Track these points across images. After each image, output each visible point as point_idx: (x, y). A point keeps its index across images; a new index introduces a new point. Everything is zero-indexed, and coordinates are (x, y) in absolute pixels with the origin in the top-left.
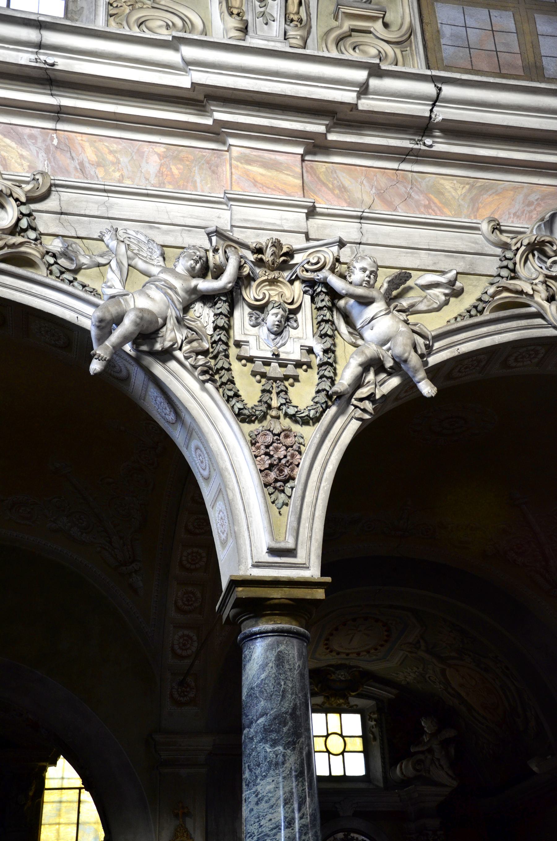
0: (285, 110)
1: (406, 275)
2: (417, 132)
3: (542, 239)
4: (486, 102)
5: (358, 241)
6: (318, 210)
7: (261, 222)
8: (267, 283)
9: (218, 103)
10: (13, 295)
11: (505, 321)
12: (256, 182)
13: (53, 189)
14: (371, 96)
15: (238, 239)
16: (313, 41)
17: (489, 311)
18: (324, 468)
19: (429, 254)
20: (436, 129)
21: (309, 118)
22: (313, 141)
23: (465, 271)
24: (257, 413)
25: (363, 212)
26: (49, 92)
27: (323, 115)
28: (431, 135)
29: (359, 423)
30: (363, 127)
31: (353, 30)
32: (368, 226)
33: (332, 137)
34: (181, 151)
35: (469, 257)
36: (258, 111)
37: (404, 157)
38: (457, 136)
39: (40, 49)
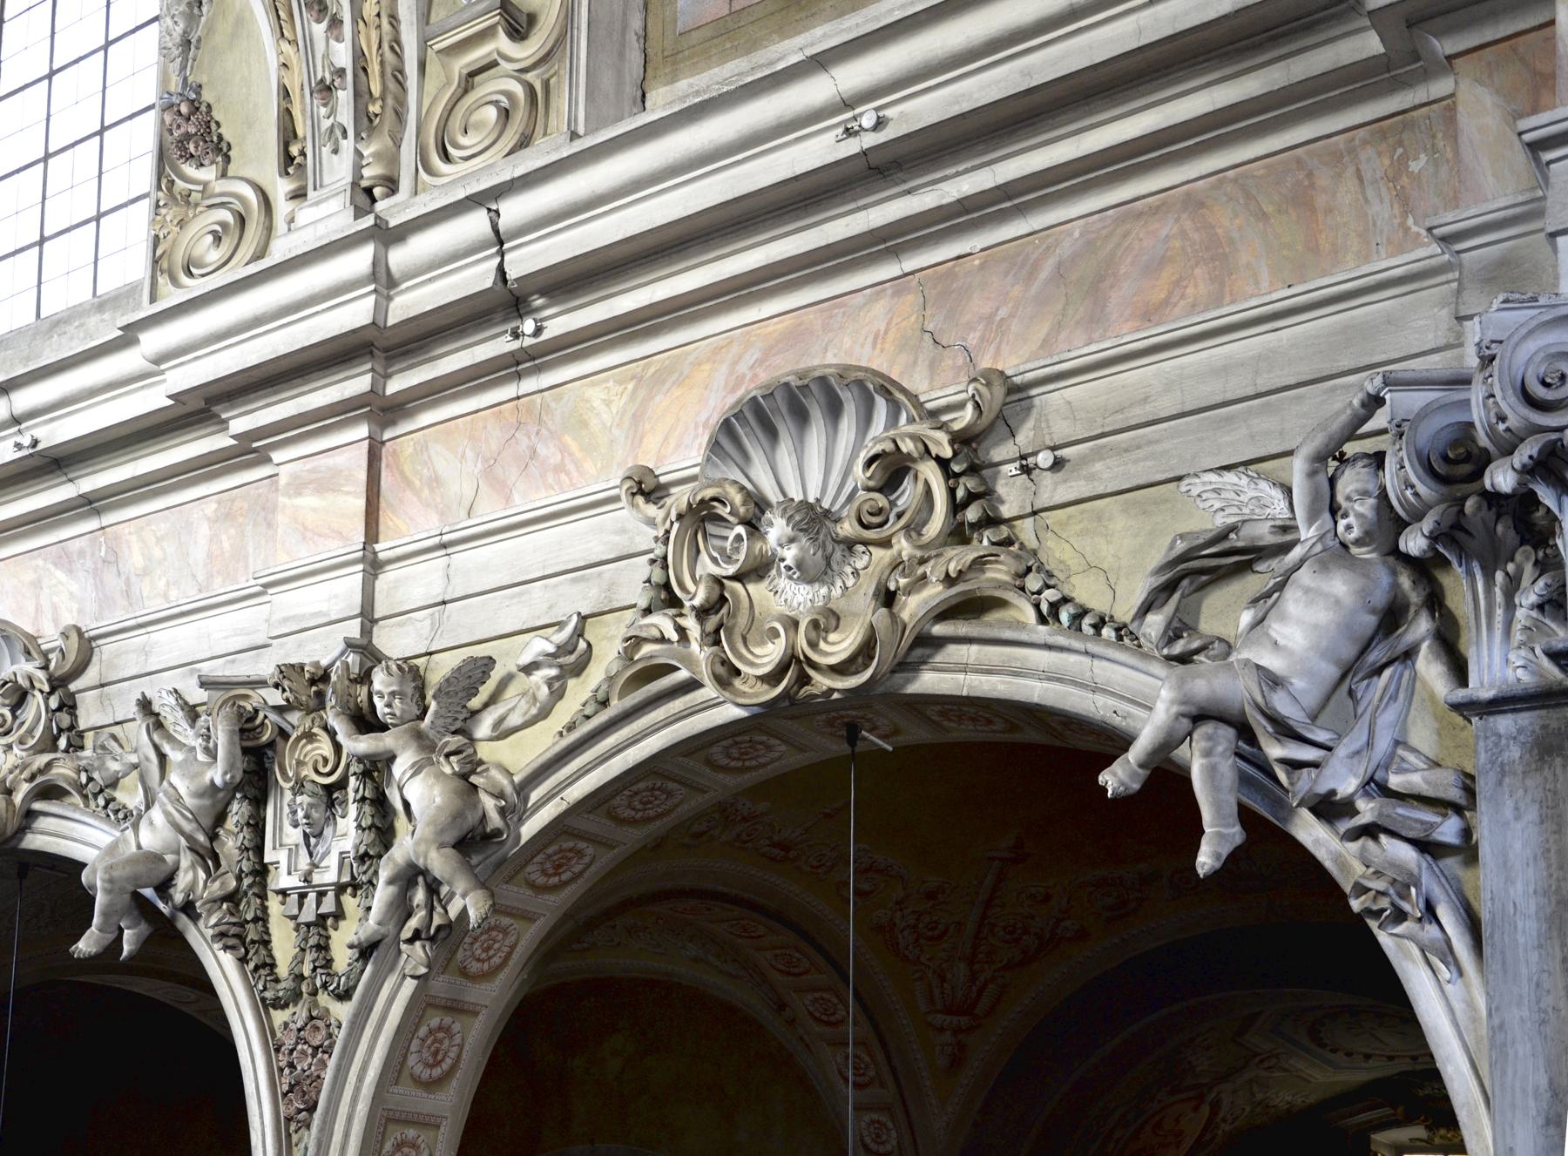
0: (307, 374)
1: (479, 663)
2: (508, 313)
3: (698, 498)
4: (576, 204)
5: (440, 599)
6: (382, 556)
7: (302, 617)
8: (304, 741)
9: (224, 405)
10: (58, 844)
11: (646, 710)
12: (306, 529)
13: (94, 645)
14: (404, 286)
15: (249, 677)
16: (410, 145)
17: (616, 698)
18: (360, 1079)
19: (546, 586)
20: (532, 294)
21: (342, 371)
22: (368, 409)
23: (596, 610)
24: (281, 994)
25: (441, 534)
26: (64, 478)
27: (356, 357)
28: (530, 309)
29: (415, 982)
30: (427, 345)
31: (472, 74)
32: (464, 558)
33: (394, 386)
34: (233, 500)
35: (610, 570)
36: (276, 393)
37: (513, 369)
38: (570, 292)
39: (20, 424)
